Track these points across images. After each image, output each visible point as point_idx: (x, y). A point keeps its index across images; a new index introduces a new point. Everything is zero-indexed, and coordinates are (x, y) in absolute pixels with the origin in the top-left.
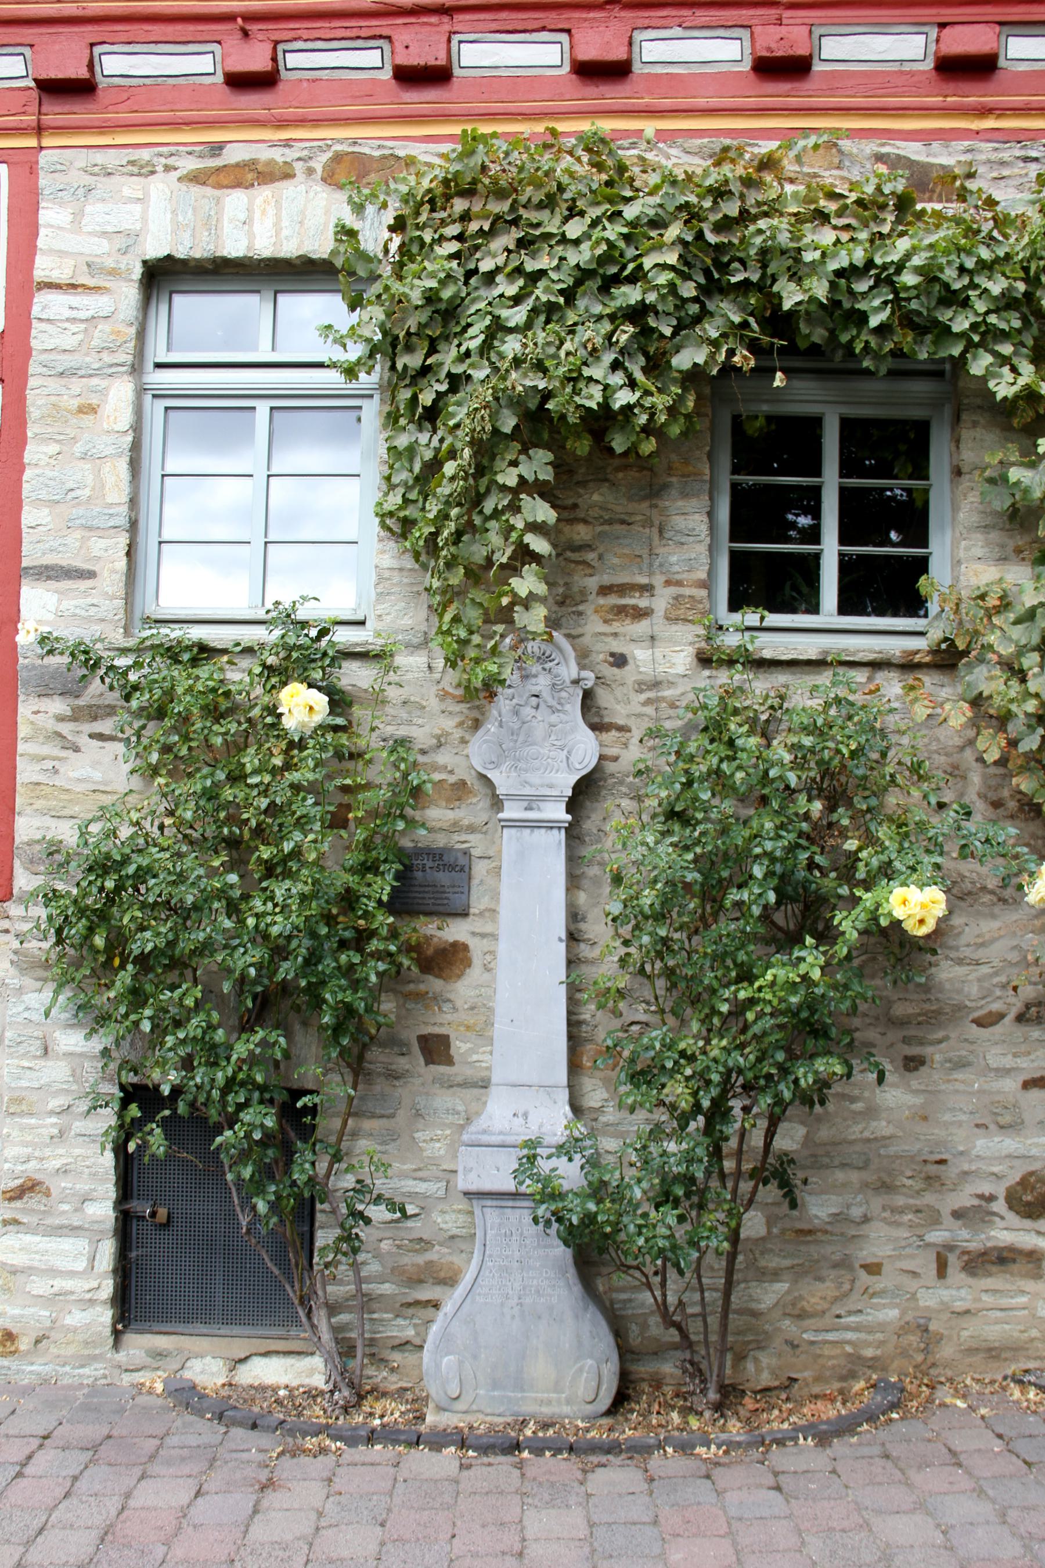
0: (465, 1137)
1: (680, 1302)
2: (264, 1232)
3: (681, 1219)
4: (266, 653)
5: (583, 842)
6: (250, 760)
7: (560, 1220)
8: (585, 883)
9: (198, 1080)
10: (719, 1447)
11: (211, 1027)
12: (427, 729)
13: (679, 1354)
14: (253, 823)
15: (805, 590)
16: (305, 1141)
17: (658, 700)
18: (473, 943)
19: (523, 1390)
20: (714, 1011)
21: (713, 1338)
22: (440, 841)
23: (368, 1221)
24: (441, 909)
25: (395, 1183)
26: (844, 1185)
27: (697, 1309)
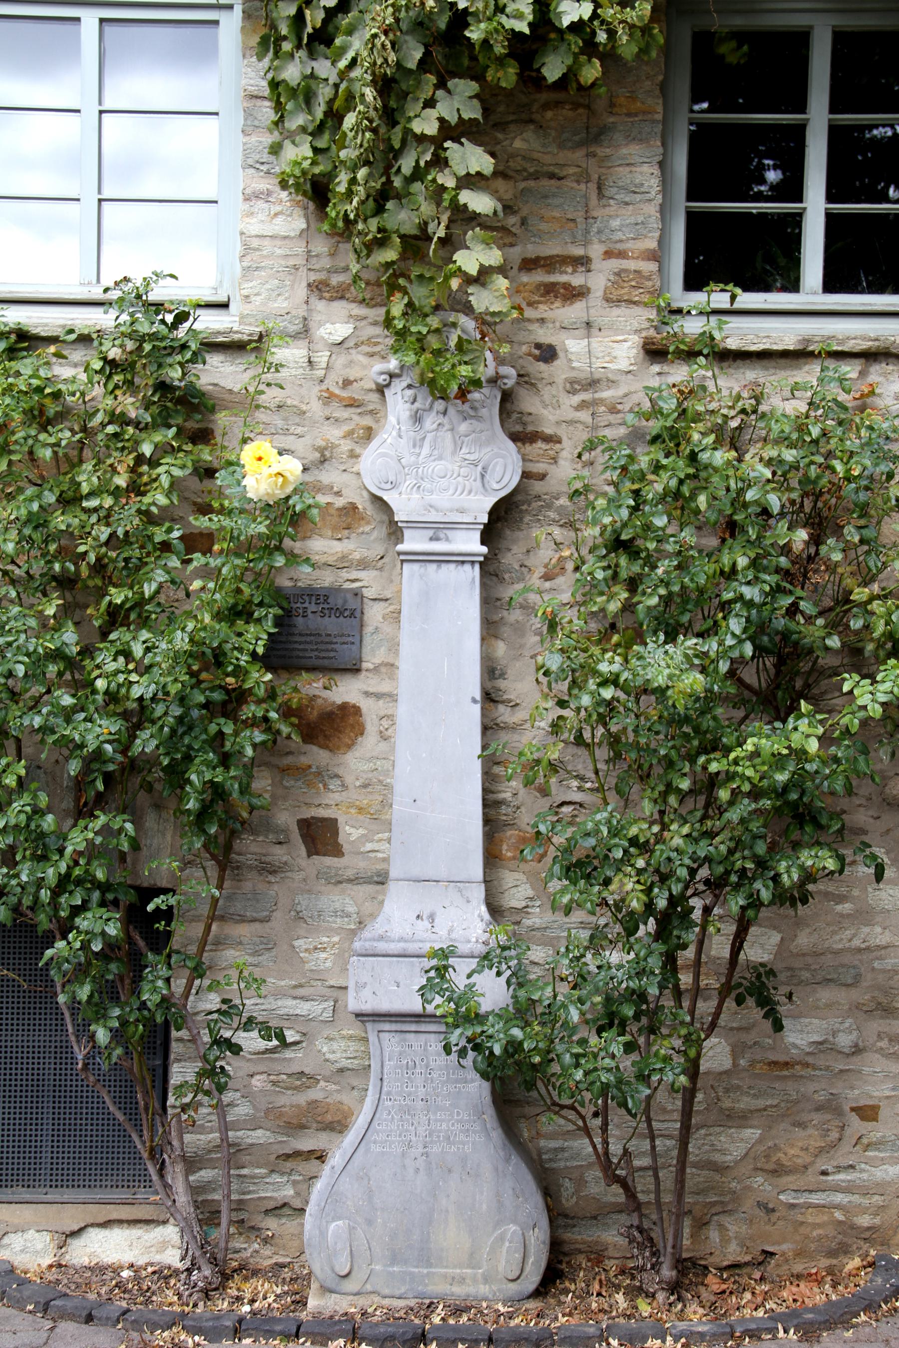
0: (357, 945)
1: (626, 1152)
2: (105, 1067)
3: (629, 1047)
4: (107, 345)
5: (502, 580)
6: (87, 478)
7: (477, 1048)
8: (506, 631)
9: (24, 878)
10: (676, 1340)
11: (37, 811)
12: (308, 440)
13: (624, 1219)
14: (92, 558)
15: (782, 261)
16: (157, 951)
17: (595, 403)
18: (367, 706)
19: (430, 1265)
20: (670, 788)
21: (667, 1198)
22: (326, 579)
23: (236, 1049)
24: (326, 662)
25: (270, 1003)
26: (829, 1006)
27: (646, 1161)
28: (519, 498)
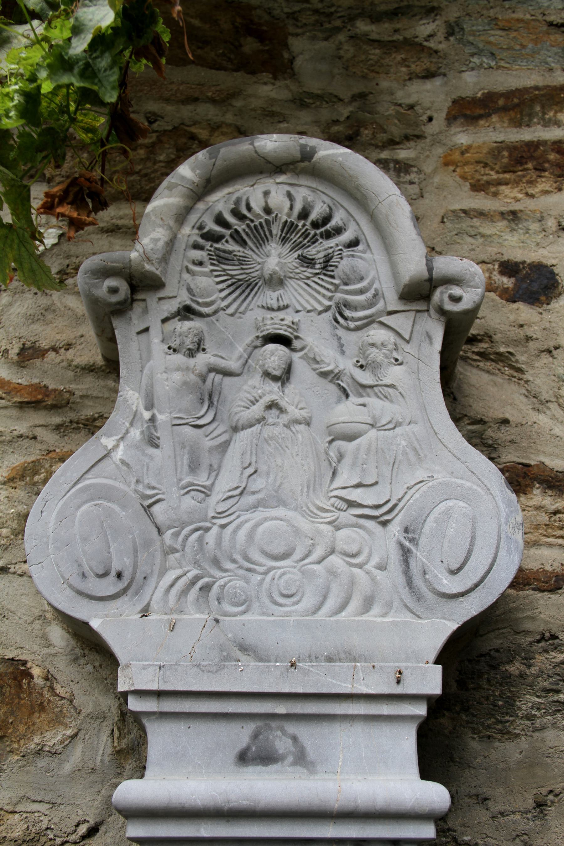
28: (493, 642)
